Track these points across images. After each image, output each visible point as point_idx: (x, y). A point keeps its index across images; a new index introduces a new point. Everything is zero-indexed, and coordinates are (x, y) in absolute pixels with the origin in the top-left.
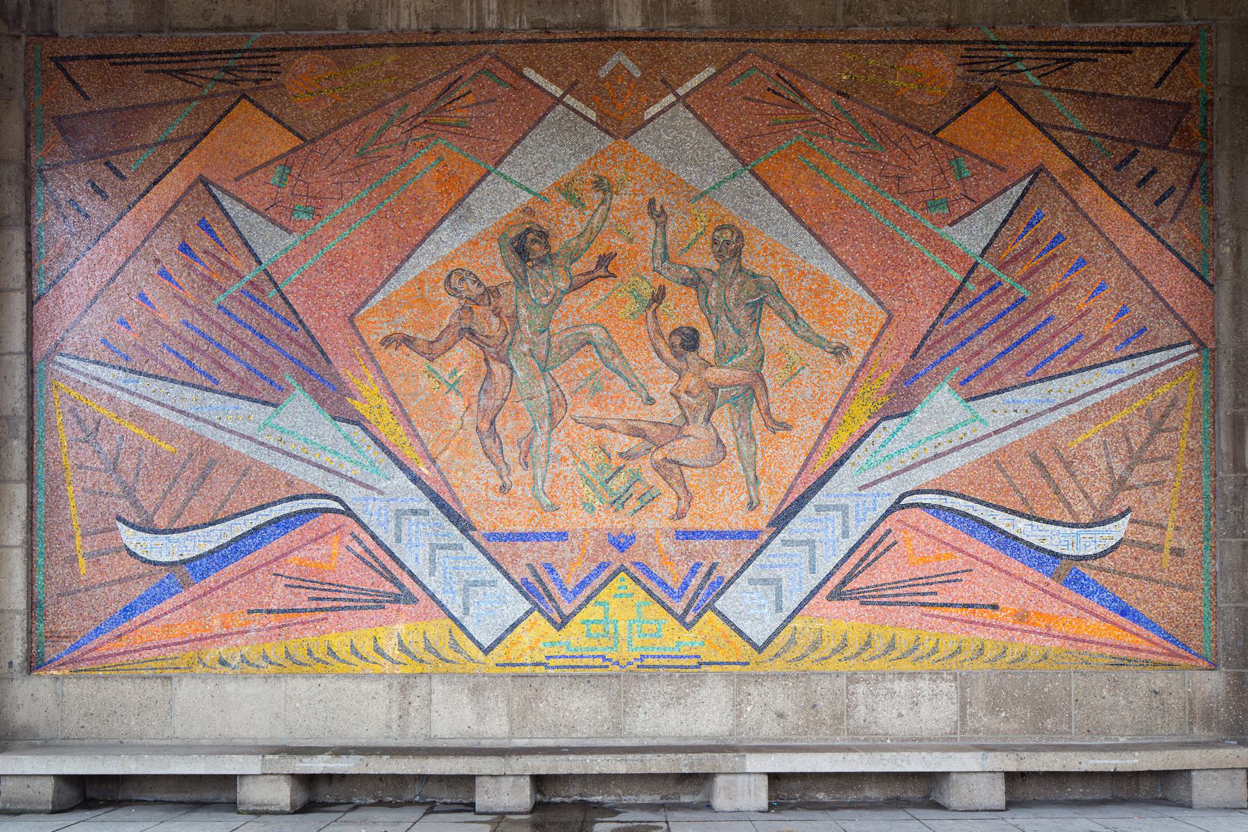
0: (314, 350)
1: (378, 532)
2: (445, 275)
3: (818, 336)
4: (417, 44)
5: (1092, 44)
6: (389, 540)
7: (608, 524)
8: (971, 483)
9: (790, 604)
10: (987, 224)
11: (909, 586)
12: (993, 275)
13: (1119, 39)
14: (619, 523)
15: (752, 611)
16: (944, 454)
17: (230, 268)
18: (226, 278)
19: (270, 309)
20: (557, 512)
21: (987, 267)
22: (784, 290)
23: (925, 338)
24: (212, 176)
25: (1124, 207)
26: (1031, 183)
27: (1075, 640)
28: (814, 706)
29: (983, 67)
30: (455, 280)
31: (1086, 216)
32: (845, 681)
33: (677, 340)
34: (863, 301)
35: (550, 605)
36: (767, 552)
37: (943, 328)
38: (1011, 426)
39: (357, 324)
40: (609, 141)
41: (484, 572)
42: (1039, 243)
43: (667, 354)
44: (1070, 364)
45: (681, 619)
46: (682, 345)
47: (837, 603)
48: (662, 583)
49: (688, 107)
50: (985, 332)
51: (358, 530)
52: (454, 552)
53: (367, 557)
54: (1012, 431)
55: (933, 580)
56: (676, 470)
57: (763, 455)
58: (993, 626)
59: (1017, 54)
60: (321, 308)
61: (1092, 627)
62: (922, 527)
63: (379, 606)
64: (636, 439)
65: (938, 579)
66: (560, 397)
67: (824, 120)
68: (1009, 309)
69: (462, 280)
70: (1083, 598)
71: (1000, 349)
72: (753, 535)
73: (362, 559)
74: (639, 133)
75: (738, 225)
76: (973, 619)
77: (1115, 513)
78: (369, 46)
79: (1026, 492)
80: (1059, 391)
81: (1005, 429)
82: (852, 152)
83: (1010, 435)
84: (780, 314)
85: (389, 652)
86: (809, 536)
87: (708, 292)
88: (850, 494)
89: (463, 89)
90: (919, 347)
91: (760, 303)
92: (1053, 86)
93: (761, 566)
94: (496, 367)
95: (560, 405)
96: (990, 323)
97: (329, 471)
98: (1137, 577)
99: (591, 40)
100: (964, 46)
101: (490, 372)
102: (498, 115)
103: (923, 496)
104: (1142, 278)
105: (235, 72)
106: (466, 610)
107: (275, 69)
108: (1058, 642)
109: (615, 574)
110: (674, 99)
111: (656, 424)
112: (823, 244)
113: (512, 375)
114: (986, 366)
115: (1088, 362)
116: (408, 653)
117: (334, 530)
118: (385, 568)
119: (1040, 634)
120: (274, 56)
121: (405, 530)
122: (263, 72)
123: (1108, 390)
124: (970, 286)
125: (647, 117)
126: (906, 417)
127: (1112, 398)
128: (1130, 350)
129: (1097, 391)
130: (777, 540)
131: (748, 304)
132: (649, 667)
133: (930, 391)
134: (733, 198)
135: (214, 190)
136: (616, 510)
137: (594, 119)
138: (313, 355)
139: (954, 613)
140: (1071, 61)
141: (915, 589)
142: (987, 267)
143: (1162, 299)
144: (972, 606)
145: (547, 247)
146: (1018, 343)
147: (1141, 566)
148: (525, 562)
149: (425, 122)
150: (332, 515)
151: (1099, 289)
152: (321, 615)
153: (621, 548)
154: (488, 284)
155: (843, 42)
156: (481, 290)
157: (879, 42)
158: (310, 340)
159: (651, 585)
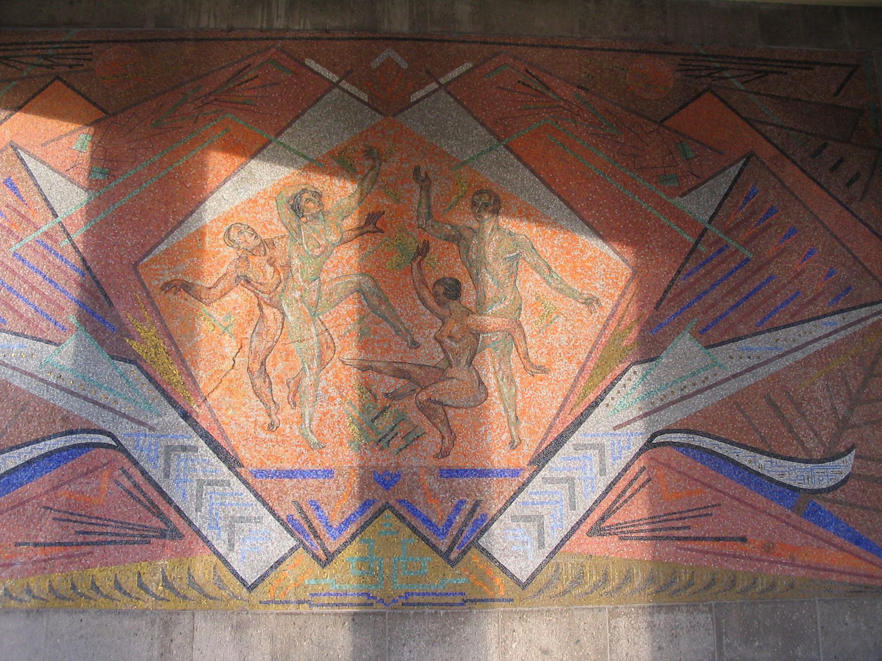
0: (99, 294)
1: (147, 467)
2: (225, 229)
3: (570, 288)
4: (214, 39)
5: (782, 61)
6: (157, 475)
7: (373, 462)
8: (715, 423)
9: (552, 541)
10: (712, 196)
11: (664, 521)
12: (720, 239)
13: (802, 58)
14: (384, 460)
15: (515, 548)
16: (689, 396)
17: (28, 220)
18: (24, 229)
19: (61, 256)
20: (324, 450)
21: (714, 231)
22: (538, 246)
23: (666, 292)
24: (20, 141)
25: (822, 187)
26: (745, 164)
27: (817, 569)
28: (578, 641)
29: (697, 73)
30: (234, 234)
31: (792, 193)
32: (607, 615)
33: (440, 290)
34: (609, 258)
35: (315, 542)
36: (529, 489)
37: (681, 283)
38: (746, 371)
39: (140, 271)
40: (379, 118)
41: (250, 508)
42: (756, 214)
43: (431, 302)
44: (792, 316)
45: (446, 556)
46: (445, 294)
47: (596, 539)
48: (427, 521)
49: (449, 93)
50: (717, 287)
51: (127, 465)
52: (221, 489)
53: (135, 492)
54: (748, 375)
55: (686, 515)
56: (440, 411)
57: (523, 397)
58: (743, 558)
59: (723, 65)
60: (108, 256)
61: (832, 557)
62: (674, 464)
63: (145, 541)
64: (402, 381)
65: (691, 514)
66: (329, 340)
67: (567, 107)
68: (736, 268)
69: (240, 232)
70: (821, 529)
71: (731, 302)
72: (515, 473)
73: (130, 493)
74: (406, 112)
75: (495, 191)
76: (724, 551)
77: (842, 450)
78: (172, 40)
79: (764, 431)
80: (785, 340)
81: (741, 373)
82: (592, 134)
83: (747, 379)
84: (535, 268)
85: (153, 588)
86: (569, 474)
87: (469, 248)
88: (606, 433)
89: (251, 74)
90: (661, 300)
91: (516, 258)
92: (755, 90)
93: (523, 503)
94: (268, 311)
95: (328, 348)
96: (721, 280)
97: (104, 407)
98: (866, 508)
99: (365, 39)
100: (680, 57)
101: (262, 316)
102: (281, 95)
103: (673, 435)
104: (844, 246)
105: (53, 59)
106: (231, 546)
107: (88, 57)
108: (802, 572)
109: (381, 511)
110: (437, 86)
111: (421, 366)
112: (572, 208)
113: (283, 319)
114: (721, 317)
115: (806, 314)
116: (172, 589)
117: (104, 465)
118: (152, 503)
119: (786, 564)
120: (88, 47)
121: (173, 465)
122: (76, 59)
123: (826, 340)
124: (702, 248)
125: (413, 99)
126: (654, 362)
127: (830, 346)
128: (840, 305)
129: (816, 340)
130: (538, 478)
131: (505, 259)
132: (413, 605)
133: (673, 339)
134: (490, 167)
135: (22, 154)
136: (382, 449)
137: (367, 100)
138: (97, 298)
139: (707, 546)
140: (767, 73)
141: (670, 524)
142: (714, 231)
143: (860, 263)
144: (723, 539)
145: (321, 205)
146: (747, 298)
147: (868, 498)
148: (291, 499)
149: (216, 100)
150: (103, 450)
151: (809, 253)
152: (88, 549)
153: (386, 486)
154: (265, 237)
155: (580, 49)
156: (258, 242)
157: (609, 50)
158: (95, 285)
159: (417, 523)
